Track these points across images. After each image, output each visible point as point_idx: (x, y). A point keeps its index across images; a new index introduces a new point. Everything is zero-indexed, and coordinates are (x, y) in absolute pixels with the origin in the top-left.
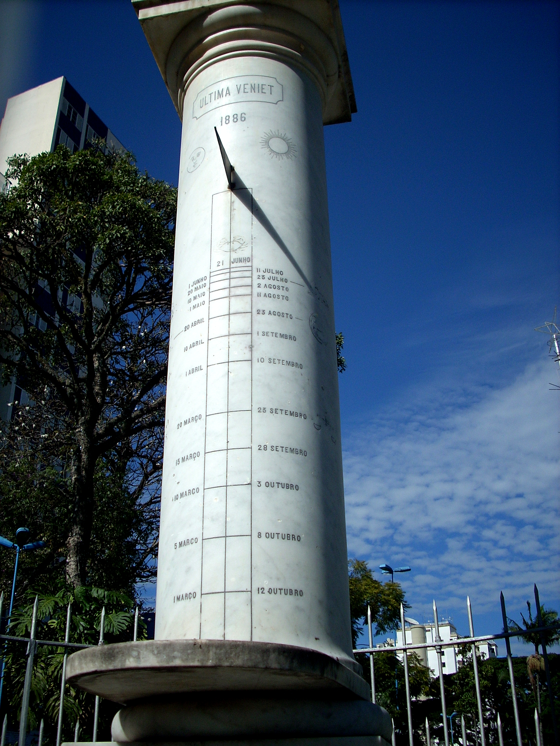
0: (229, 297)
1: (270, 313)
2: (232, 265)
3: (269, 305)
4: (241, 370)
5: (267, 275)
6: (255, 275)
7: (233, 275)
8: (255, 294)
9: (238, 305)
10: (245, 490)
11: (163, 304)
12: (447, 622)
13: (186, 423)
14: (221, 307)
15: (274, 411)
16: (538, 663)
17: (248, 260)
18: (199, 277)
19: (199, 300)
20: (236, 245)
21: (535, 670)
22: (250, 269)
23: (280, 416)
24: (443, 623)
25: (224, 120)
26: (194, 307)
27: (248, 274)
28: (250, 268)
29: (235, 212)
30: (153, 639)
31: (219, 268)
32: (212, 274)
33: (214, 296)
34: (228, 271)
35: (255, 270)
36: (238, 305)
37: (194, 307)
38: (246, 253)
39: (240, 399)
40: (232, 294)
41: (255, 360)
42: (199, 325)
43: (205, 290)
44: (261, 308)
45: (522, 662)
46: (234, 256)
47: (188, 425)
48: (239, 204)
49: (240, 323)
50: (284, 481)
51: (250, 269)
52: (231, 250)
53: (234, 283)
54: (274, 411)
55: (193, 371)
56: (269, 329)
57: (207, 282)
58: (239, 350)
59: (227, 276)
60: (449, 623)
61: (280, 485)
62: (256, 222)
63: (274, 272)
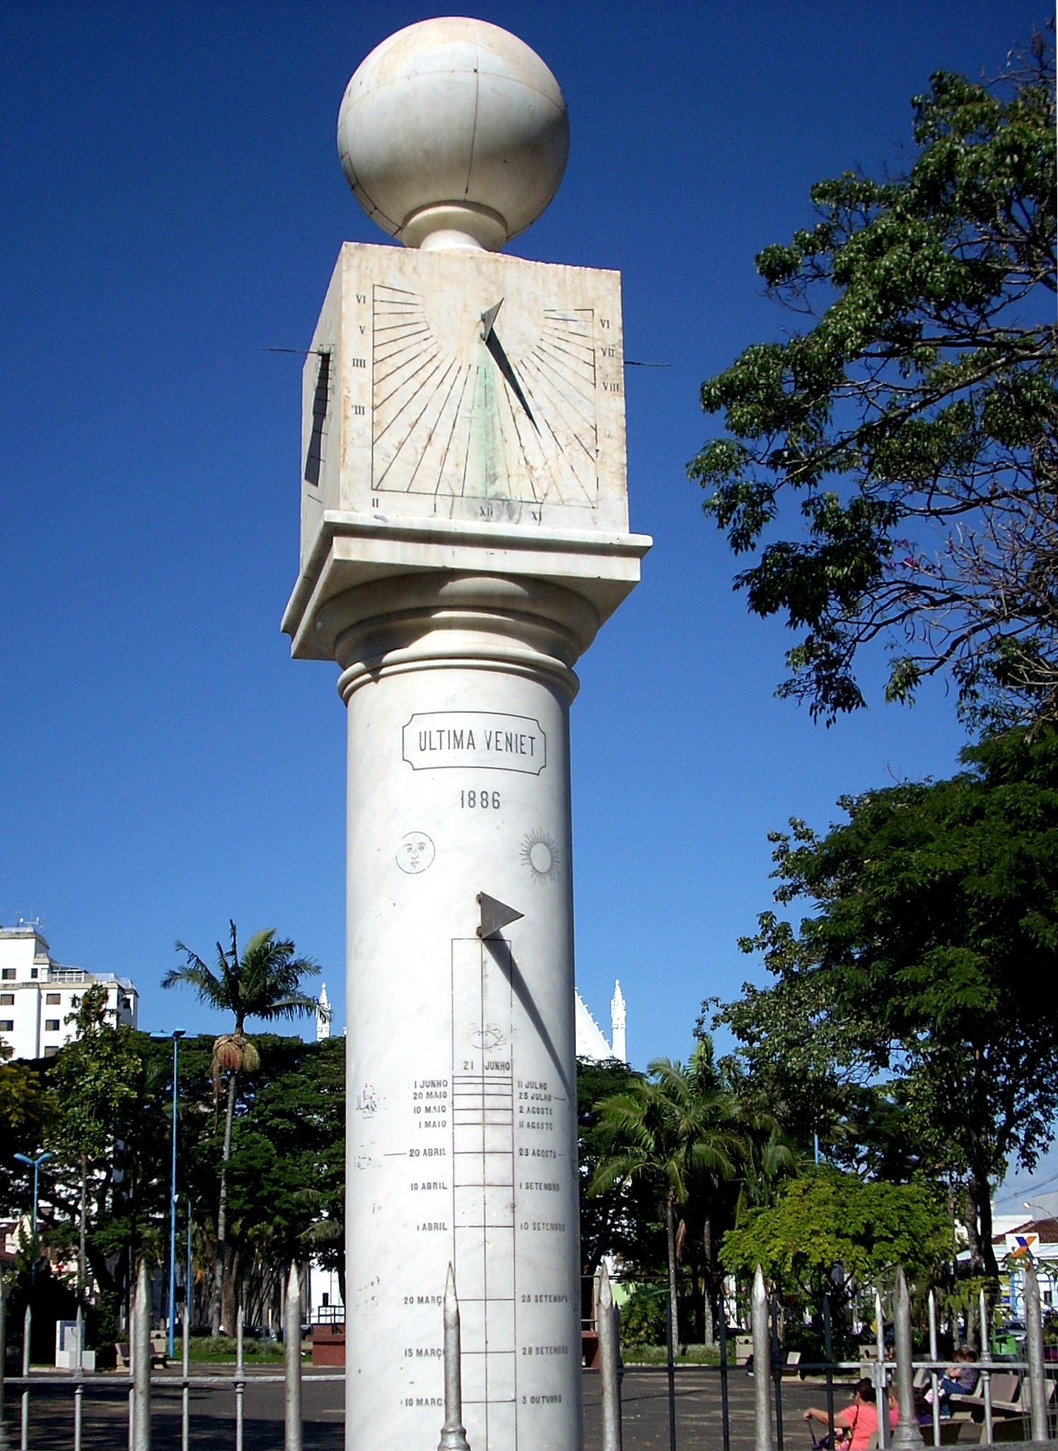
0: (483, 1124)
2: (487, 1073)
3: (532, 1140)
4: (500, 1240)
5: (531, 1092)
6: (517, 1091)
7: (488, 1089)
8: (516, 1124)
9: (497, 1139)
10: (508, 1409)
12: (30, 930)
13: (421, 1300)
14: (470, 1138)
15: (539, 1299)
16: (239, 1054)
17: (507, 1066)
18: (436, 1078)
19: (434, 1117)
20: (490, 1039)
21: (227, 1064)
22: (509, 1081)
23: (545, 1304)
24: (21, 930)
25: (466, 798)
26: (427, 1124)
27: (507, 1090)
29: (487, 981)
30: (54, 1363)
33: (461, 1117)
35: (515, 1084)
36: (497, 1139)
37: (427, 1124)
38: (502, 1056)
39: (501, 1283)
40: (487, 1120)
41: (518, 1226)
42: (435, 1158)
43: (445, 1102)
44: (524, 1147)
45: (201, 1047)
46: (491, 1057)
47: (424, 1305)
48: (493, 967)
49: (498, 1168)
50: (548, 1394)
51: (509, 1081)
52: (484, 1047)
53: (490, 1101)
54: (539, 1299)
55: (430, 1227)
56: (533, 1180)
57: (448, 1089)
58: (499, 1214)
60: (35, 933)
62: (517, 1001)
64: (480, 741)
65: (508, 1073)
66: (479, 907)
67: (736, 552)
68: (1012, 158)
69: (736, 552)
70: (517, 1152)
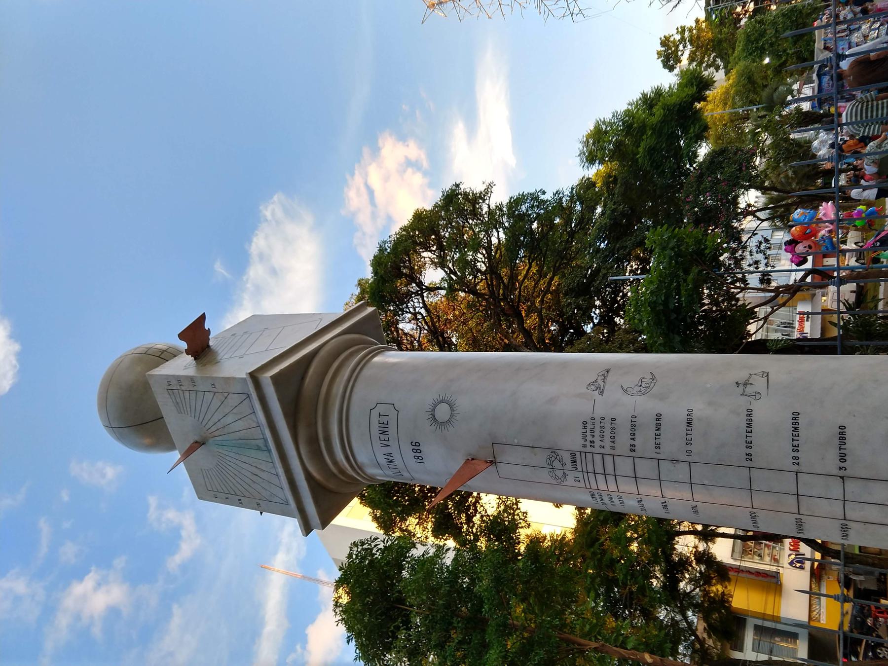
1: (633, 439)
2: (580, 469)
6: (588, 449)
8: (612, 452)
11: (492, 281)
17: (573, 455)
27: (589, 456)
28: (583, 454)
31: (582, 481)
32: (588, 486)
34: (585, 474)
51: (583, 454)
53: (599, 469)
59: (591, 476)
61: (843, 447)
63: (584, 430)
64: (387, 450)
65: (578, 454)
66: (565, 506)
67: (751, 384)
68: (624, 207)
69: (751, 384)
70: (633, 454)
